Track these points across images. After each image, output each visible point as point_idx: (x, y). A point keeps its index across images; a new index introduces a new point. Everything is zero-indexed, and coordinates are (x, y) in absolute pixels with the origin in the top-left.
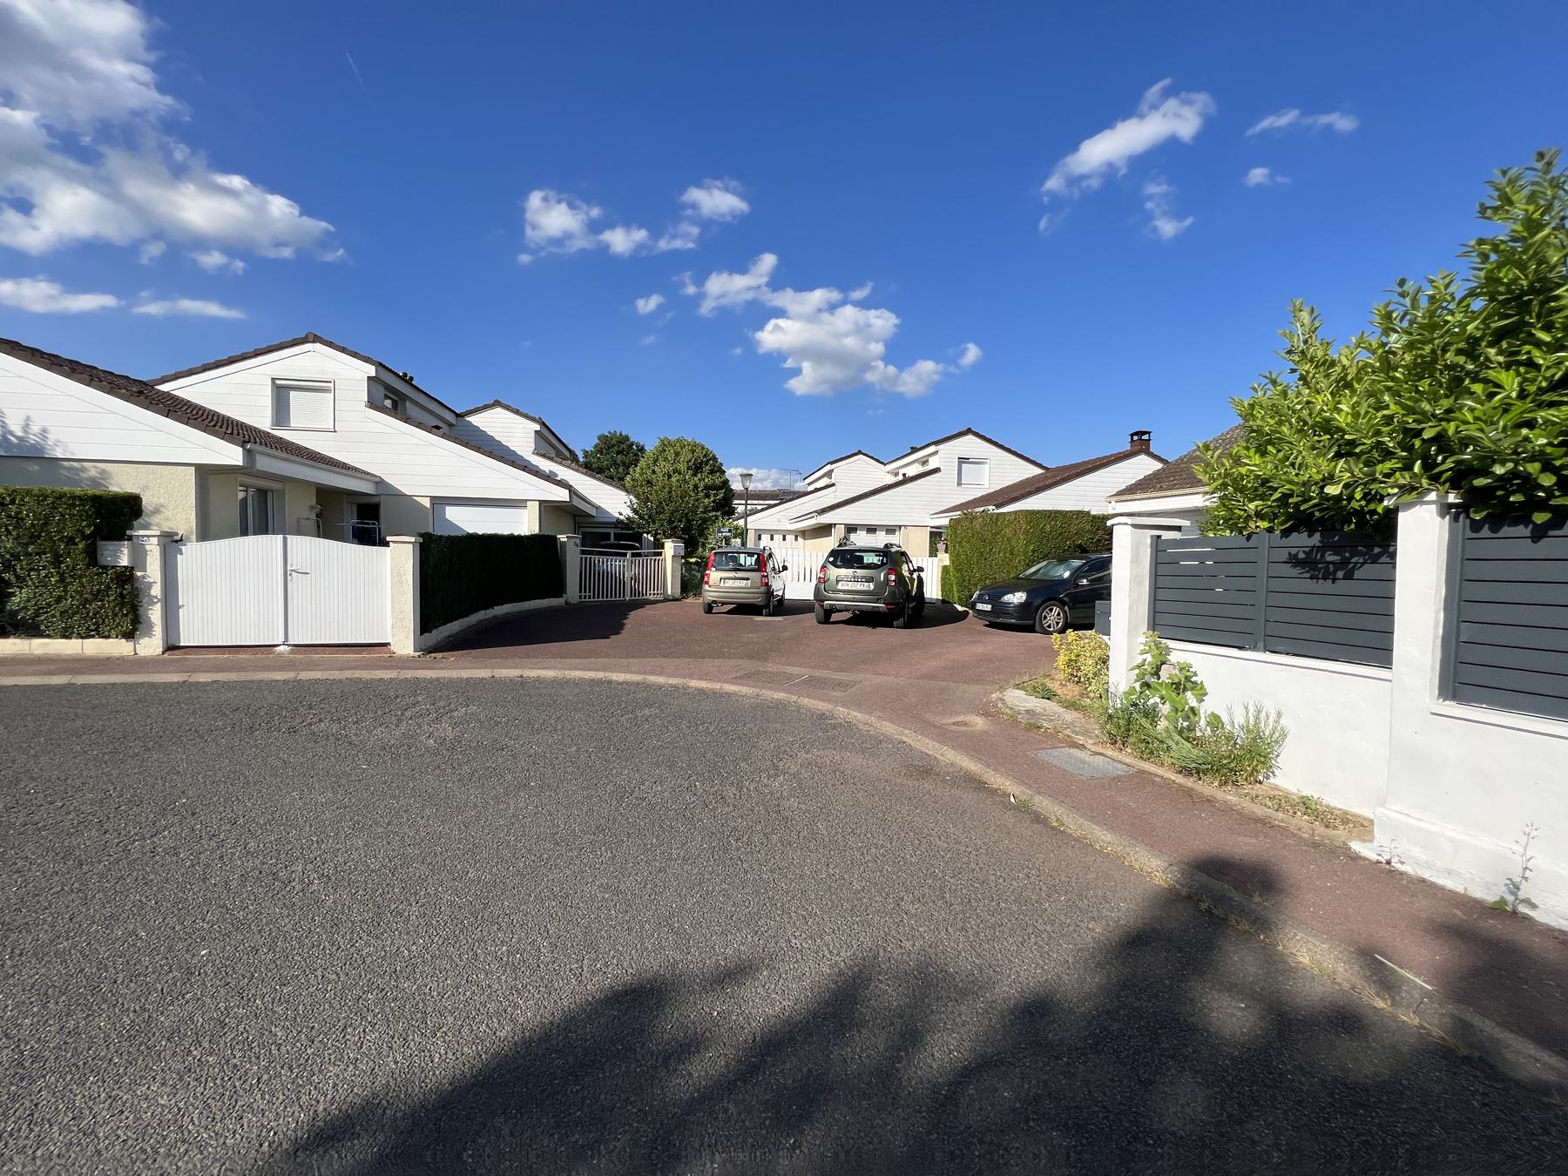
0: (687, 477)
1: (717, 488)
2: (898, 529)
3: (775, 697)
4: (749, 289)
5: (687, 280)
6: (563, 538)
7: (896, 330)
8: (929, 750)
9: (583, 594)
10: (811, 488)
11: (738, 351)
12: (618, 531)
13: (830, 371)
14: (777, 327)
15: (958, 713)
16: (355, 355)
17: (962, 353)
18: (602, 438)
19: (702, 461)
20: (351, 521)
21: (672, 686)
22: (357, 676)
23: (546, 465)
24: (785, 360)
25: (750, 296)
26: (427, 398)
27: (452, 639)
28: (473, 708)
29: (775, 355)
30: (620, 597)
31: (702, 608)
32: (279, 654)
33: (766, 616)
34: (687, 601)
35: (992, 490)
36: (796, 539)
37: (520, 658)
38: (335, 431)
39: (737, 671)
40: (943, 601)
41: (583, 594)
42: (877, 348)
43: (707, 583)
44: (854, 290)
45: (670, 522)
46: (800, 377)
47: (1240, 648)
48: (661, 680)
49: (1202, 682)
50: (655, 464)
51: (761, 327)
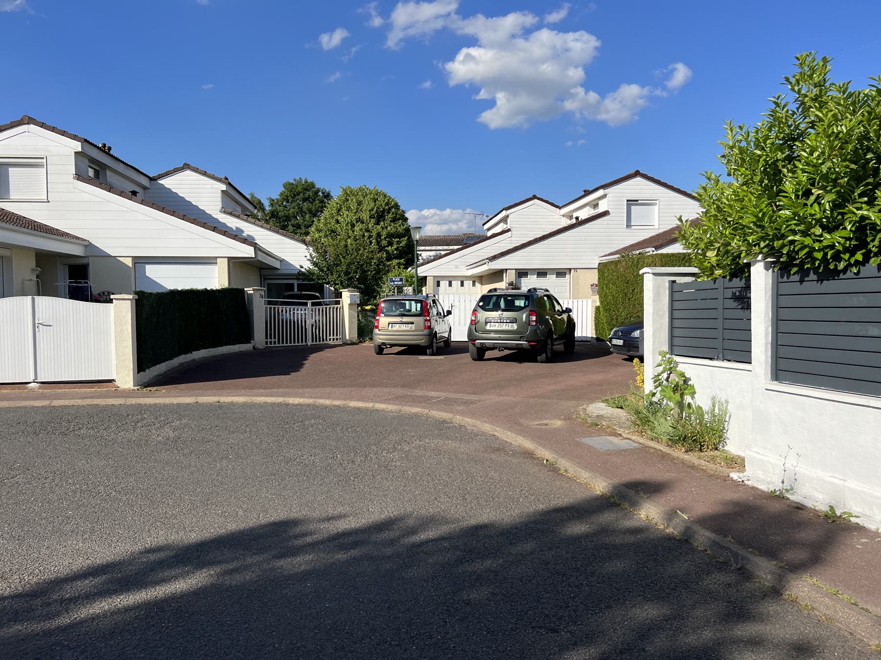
0: (370, 226)
1: (400, 236)
2: (568, 272)
3: (413, 411)
4: (437, 17)
5: (373, 13)
6: (249, 290)
7: (596, 53)
8: (508, 439)
9: (269, 340)
10: (489, 234)
11: (427, 85)
12: (300, 282)
13: (524, 101)
14: (469, 57)
15: (546, 419)
16: (63, 133)
17: (671, 74)
18: (289, 186)
19: (384, 209)
20: (64, 281)
21: (335, 406)
22: (94, 403)
23: (233, 223)
24: (478, 91)
25: (439, 24)
26: (125, 166)
27: (161, 377)
28: (184, 421)
29: (467, 86)
30: (302, 342)
31: (374, 351)
32: (31, 389)
33: (430, 355)
34: (364, 344)
35: (661, 231)
36: (474, 285)
37: (217, 389)
38: (48, 202)
39: (389, 395)
40: (598, 339)
41: (269, 340)
42: (576, 74)
43: (377, 327)
44: (550, 13)
45: (347, 273)
46: (494, 110)
47: (711, 359)
48: (327, 402)
49: (693, 385)
50: (338, 214)
51: (451, 57)
